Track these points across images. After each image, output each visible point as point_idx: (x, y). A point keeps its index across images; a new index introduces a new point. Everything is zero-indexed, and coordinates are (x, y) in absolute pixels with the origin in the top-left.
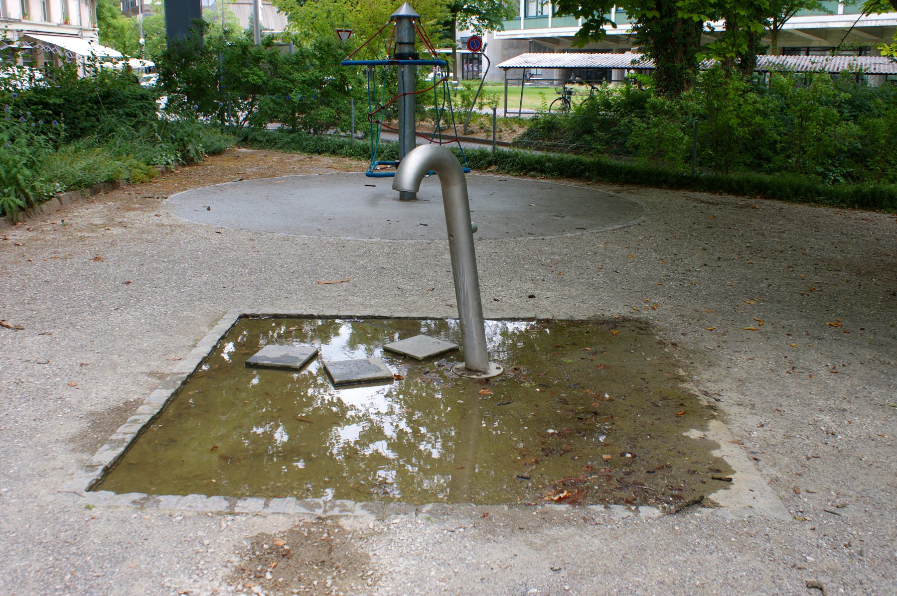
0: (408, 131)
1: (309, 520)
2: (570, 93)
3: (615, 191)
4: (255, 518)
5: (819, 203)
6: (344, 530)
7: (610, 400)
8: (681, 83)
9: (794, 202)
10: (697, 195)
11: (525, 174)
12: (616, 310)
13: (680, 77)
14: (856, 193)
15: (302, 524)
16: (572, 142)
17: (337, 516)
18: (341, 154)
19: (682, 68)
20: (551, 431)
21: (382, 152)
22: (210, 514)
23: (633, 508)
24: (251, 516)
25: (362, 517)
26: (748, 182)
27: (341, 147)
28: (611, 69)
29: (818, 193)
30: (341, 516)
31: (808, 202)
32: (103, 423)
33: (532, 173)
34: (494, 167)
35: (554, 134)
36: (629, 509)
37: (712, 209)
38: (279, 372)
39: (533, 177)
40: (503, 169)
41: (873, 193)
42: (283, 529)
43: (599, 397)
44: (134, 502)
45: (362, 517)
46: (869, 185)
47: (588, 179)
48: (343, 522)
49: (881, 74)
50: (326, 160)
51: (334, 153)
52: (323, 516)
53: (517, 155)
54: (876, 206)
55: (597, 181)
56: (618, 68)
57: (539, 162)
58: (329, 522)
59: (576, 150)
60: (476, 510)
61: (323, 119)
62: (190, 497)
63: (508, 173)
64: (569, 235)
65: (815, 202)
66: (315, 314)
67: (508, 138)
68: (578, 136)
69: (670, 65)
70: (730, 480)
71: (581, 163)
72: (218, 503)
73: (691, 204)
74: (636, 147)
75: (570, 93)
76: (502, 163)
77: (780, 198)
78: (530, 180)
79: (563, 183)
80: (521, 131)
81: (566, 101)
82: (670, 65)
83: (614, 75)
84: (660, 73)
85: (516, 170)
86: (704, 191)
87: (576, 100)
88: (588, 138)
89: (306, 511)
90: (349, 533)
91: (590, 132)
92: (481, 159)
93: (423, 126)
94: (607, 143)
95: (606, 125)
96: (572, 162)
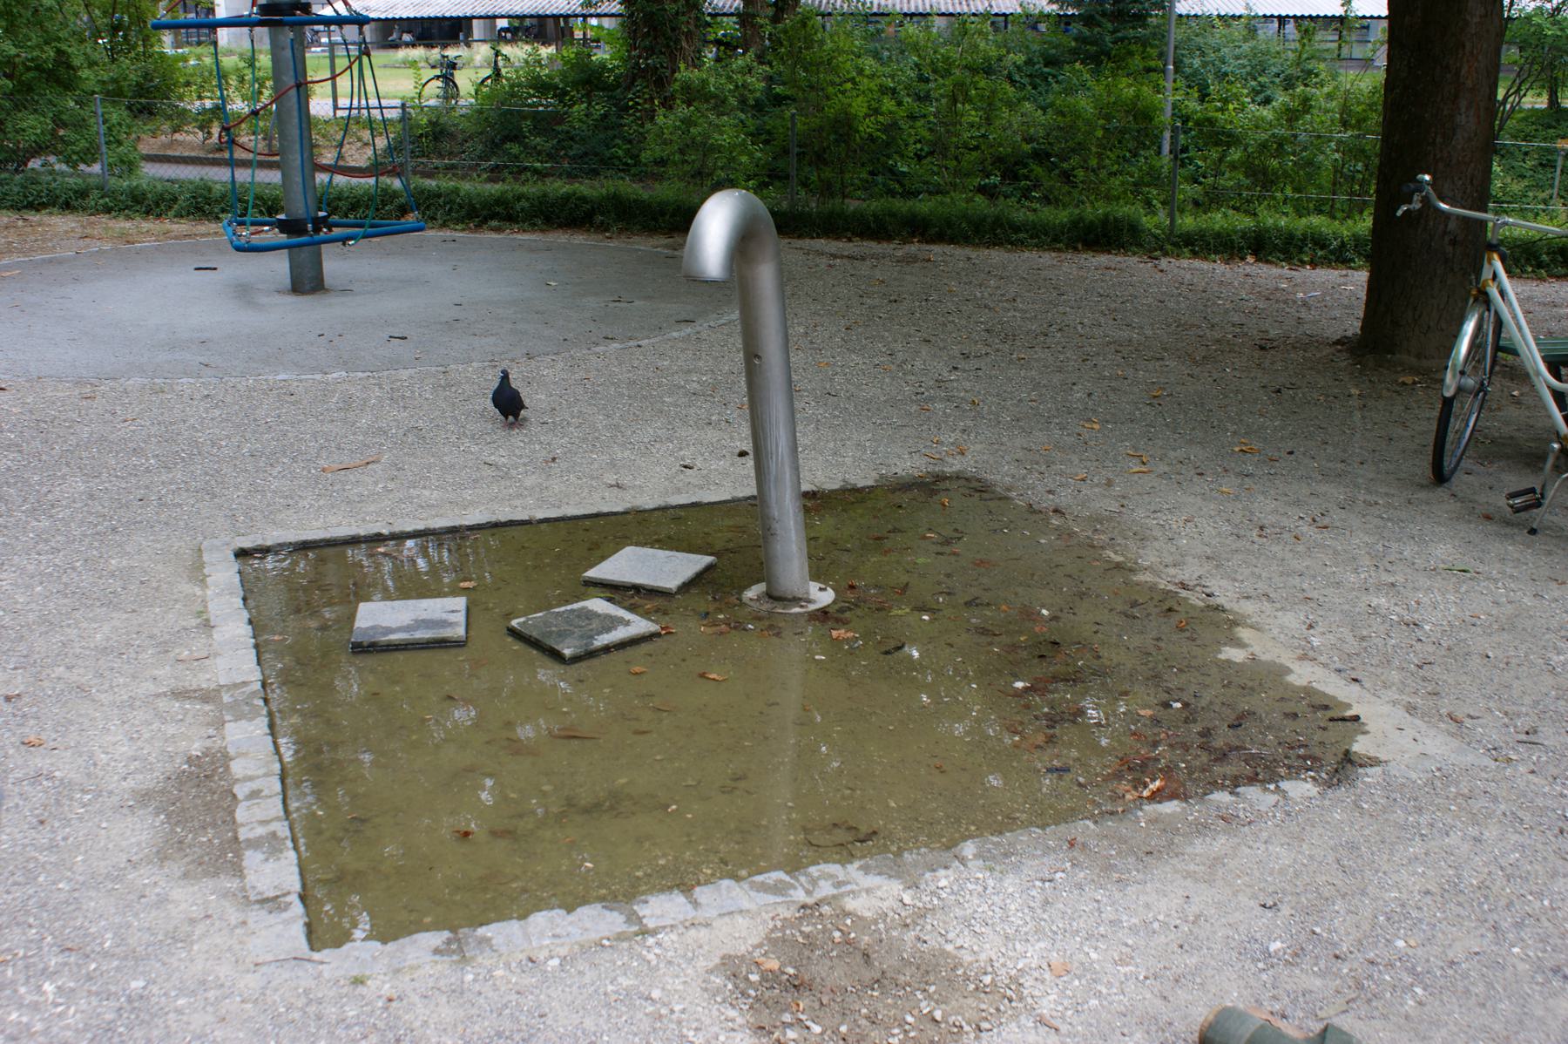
0: (295, 159)
1: (788, 914)
2: (453, 66)
3: (666, 246)
4: (693, 932)
5: (1019, 245)
6: (861, 918)
7: (1054, 618)
8: (677, 41)
9: (978, 245)
10: (806, 243)
11: (478, 227)
12: (907, 464)
13: (673, 30)
14: (1076, 223)
15: (779, 924)
16: (484, 157)
17: (834, 897)
18: (84, 209)
19: (677, 13)
20: (1019, 685)
21: (175, 200)
22: (605, 942)
23: (1272, 787)
24: (681, 930)
25: (879, 887)
26: (893, 215)
27: (83, 194)
28: (468, 20)
29: (1017, 229)
30: (843, 895)
31: (1000, 244)
32: (195, 803)
33: (494, 223)
34: (411, 218)
35: (446, 145)
36: (1267, 789)
37: (864, 268)
38: (425, 654)
39: (498, 230)
40: (433, 218)
41: (1105, 221)
42: (756, 941)
43: (1029, 614)
44: (437, 951)
45: (879, 887)
46: (1095, 210)
47: (603, 228)
48: (850, 904)
49: (951, 15)
50: (61, 223)
51: (67, 207)
52: (810, 901)
53: (456, 191)
54: (1110, 244)
55: (621, 231)
56: (481, 17)
57: (500, 201)
58: (826, 909)
59: (495, 174)
60: (1053, 835)
61: (30, 137)
62: (539, 919)
63: (444, 225)
64: (675, 334)
65: (1012, 243)
66: (385, 531)
67: (358, 157)
68: (494, 147)
69: (655, 8)
70: (1356, 718)
71: (583, 199)
72: (597, 921)
73: (823, 262)
74: (662, 162)
75: (453, 66)
76: (428, 208)
77: (952, 241)
78: (495, 236)
79: (561, 238)
80: (381, 143)
81: (448, 79)
82: (655, 8)
83: (478, 29)
84: (634, 23)
85: (458, 221)
86: (818, 237)
87: (465, 81)
88: (515, 149)
89: (779, 899)
90: (876, 922)
91: (516, 138)
92: (384, 203)
93: (181, 143)
94: (551, 157)
95: (545, 124)
96: (567, 198)
